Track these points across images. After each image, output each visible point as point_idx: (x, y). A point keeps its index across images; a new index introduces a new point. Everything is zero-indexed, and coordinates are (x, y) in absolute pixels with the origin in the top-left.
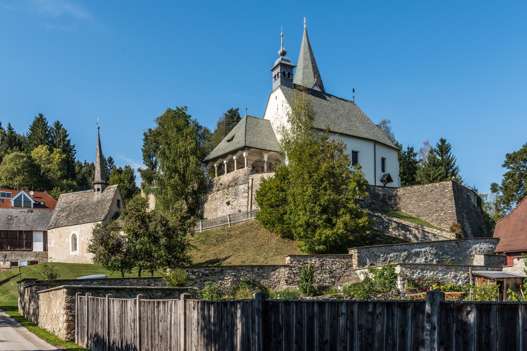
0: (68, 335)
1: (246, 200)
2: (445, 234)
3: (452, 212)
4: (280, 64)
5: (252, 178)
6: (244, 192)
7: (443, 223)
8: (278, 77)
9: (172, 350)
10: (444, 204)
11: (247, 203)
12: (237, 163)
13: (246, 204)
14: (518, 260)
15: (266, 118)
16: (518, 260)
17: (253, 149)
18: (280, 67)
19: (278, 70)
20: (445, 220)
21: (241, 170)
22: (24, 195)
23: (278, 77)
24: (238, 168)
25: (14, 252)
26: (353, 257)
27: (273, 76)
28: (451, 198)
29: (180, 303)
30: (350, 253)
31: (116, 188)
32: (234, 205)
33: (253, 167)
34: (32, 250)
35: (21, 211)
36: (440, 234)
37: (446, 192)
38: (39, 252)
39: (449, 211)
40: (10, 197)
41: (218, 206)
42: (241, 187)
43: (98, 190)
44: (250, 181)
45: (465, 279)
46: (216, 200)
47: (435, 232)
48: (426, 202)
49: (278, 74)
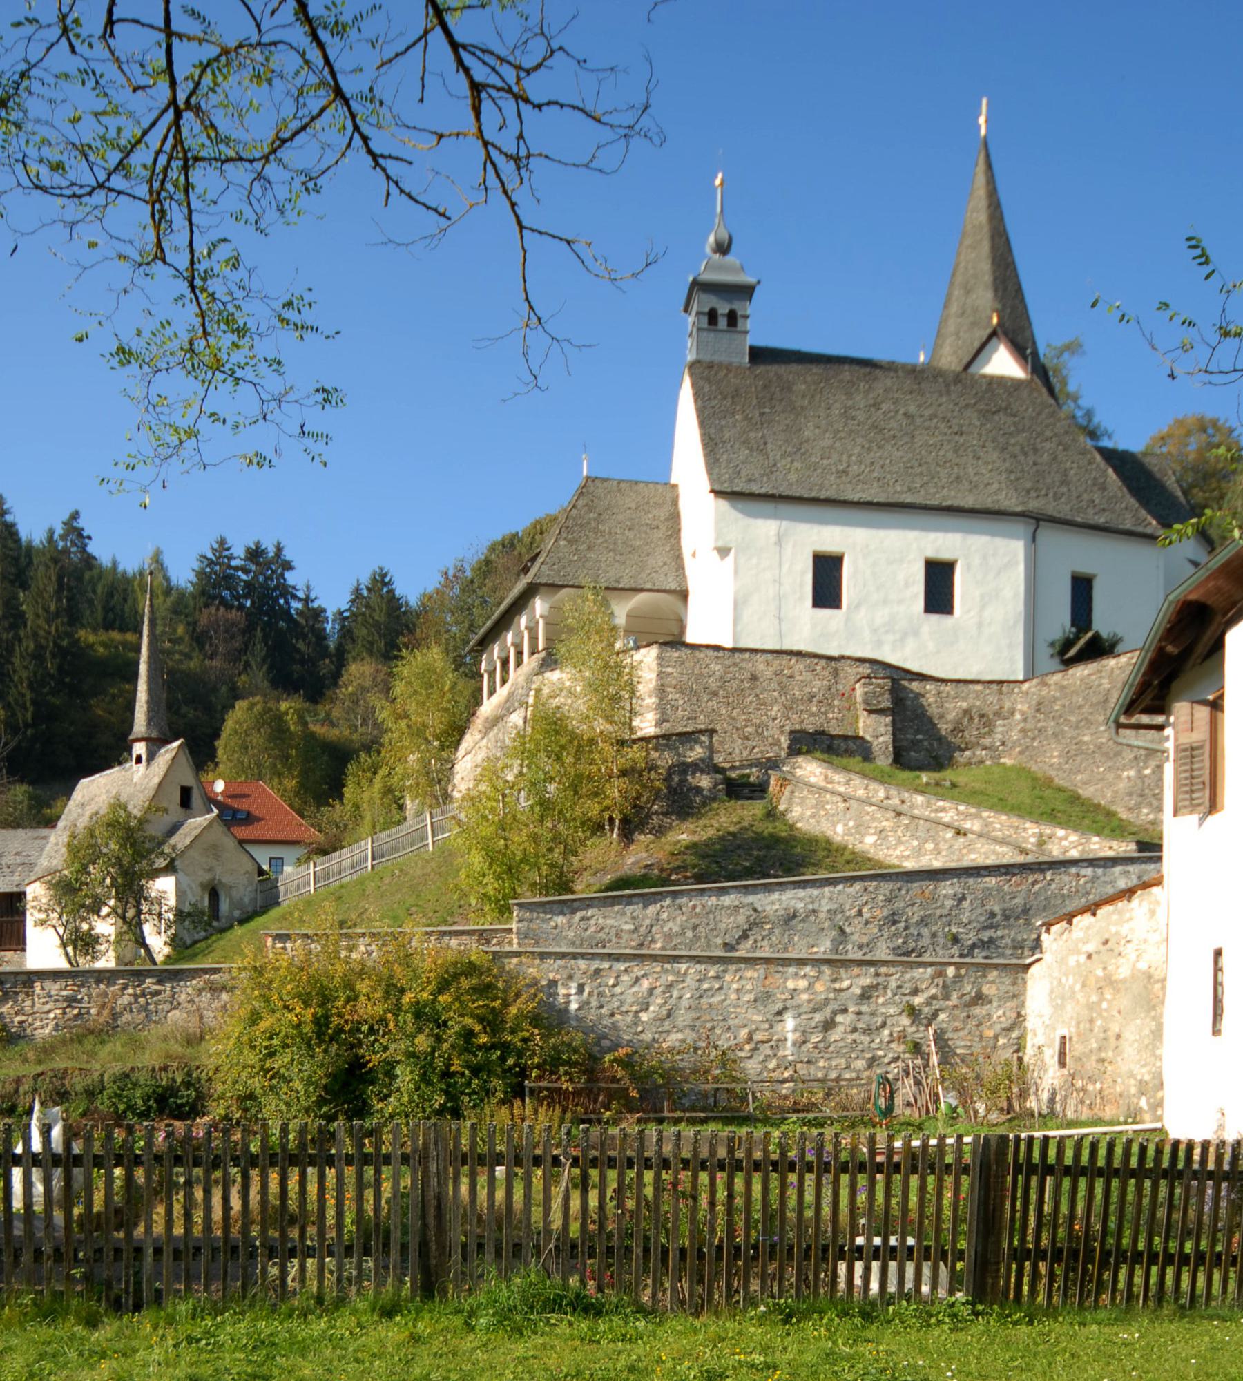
2: (1096, 846)
45: (815, 1010)
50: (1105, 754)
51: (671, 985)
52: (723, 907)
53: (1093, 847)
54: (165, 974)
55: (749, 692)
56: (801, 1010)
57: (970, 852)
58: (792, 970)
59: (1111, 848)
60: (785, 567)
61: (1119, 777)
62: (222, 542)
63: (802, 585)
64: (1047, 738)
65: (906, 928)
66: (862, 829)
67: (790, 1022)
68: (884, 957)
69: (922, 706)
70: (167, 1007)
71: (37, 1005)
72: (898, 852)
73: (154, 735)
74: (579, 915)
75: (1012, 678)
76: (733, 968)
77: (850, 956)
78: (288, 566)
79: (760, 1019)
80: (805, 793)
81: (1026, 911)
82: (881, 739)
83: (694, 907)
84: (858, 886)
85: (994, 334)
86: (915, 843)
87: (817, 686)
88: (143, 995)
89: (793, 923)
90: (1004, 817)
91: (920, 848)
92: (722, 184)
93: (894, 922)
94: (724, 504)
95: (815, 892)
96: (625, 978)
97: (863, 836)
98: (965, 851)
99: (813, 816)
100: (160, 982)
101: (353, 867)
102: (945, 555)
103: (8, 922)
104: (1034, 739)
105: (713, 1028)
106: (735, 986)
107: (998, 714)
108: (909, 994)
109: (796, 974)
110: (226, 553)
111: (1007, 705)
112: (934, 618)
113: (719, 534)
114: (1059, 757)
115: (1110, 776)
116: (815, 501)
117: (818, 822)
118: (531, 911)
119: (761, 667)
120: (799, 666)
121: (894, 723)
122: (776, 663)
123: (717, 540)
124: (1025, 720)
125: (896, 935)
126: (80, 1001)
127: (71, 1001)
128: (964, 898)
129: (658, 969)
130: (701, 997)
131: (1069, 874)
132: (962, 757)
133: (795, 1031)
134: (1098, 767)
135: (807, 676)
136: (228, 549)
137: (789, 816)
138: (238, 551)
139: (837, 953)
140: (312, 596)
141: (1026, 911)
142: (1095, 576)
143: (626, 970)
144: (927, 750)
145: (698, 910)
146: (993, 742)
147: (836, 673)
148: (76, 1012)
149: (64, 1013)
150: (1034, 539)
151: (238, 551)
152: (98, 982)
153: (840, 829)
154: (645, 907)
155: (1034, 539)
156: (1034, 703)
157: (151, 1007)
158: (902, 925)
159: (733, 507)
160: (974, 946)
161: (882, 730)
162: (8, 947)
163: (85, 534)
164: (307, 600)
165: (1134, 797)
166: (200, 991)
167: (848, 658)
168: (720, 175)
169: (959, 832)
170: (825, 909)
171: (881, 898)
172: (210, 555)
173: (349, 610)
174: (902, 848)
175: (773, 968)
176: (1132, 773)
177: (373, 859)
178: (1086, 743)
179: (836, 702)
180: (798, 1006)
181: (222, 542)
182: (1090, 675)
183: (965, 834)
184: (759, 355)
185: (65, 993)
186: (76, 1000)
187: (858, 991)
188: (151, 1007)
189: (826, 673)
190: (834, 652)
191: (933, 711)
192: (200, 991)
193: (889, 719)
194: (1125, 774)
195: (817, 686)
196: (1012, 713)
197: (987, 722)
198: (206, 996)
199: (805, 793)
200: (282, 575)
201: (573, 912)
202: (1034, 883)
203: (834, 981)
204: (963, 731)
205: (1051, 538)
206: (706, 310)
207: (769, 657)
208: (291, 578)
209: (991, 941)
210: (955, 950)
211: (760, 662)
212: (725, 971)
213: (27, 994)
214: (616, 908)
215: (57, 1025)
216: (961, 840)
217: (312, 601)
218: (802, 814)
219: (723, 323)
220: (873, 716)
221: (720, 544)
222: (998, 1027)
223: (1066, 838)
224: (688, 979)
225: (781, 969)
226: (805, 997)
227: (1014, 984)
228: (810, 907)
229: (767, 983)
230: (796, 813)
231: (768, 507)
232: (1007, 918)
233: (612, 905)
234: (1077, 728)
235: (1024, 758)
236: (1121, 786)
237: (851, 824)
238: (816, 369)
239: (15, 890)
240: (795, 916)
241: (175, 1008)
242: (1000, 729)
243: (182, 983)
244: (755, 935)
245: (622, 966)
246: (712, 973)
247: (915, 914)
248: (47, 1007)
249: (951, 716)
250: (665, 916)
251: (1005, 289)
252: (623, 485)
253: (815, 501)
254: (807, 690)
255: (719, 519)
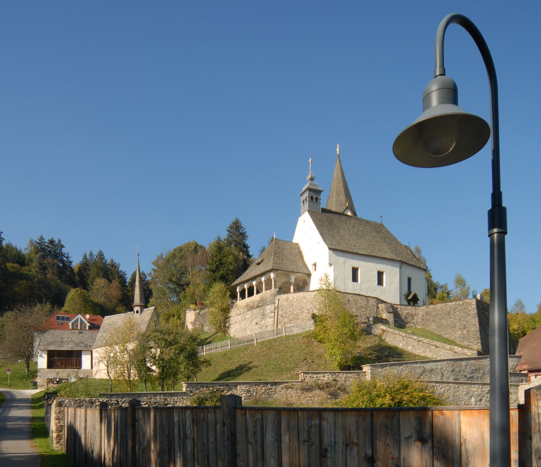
0: (57, 444)
1: (273, 319)
2: (466, 351)
3: (476, 330)
4: (309, 189)
5: (278, 298)
6: (271, 312)
7: (466, 340)
8: (306, 201)
9: (271, 462)
10: (467, 322)
11: (273, 322)
12: (265, 284)
13: (272, 323)
14: (536, 377)
15: (294, 241)
16: (536, 377)
17: (280, 271)
18: (308, 192)
19: (306, 195)
20: (468, 338)
21: (268, 291)
22: (80, 318)
23: (306, 201)
24: (266, 290)
25: (65, 370)
26: (366, 374)
27: (302, 200)
28: (475, 316)
29: (83, 410)
30: (364, 370)
31: (152, 311)
32: (261, 325)
33: (280, 289)
34: (81, 368)
35: (72, 332)
36: (462, 352)
37: (469, 310)
38: (87, 370)
39: (473, 329)
40: (69, 320)
41: (248, 326)
42: (268, 307)
43: (137, 312)
44: (277, 301)
45: (478, 396)
46: (246, 320)
47: (456, 349)
48: (449, 320)
49: (306, 199)
50: (451, 327)
51: (448, 390)
52: (417, 367)
53: (465, 352)
54: (273, 384)
55: (347, 304)
56: (476, 396)
57: (440, 352)
58: (473, 386)
59: (470, 352)
60: (346, 270)
61: (456, 333)
62: (42, 237)
64: (430, 322)
65: (456, 373)
66: (408, 345)
67: (473, 400)
68: (452, 381)
69: (397, 311)
70: (274, 393)
71: (238, 392)
72: (418, 351)
73: (143, 305)
74: (384, 368)
75: (397, 304)
76: (461, 385)
77: (444, 381)
78: (62, 246)
79: (467, 398)
80: (390, 334)
81: (479, 369)
82: (391, 320)
83: (411, 367)
84: (446, 362)
85: (347, 208)
86: (424, 349)
87: (364, 304)
88: (267, 389)
89: (432, 371)
90: (440, 343)
91: (425, 350)
92: (311, 161)
93: (454, 372)
94: (331, 252)
95: (437, 363)
96: (438, 388)
97: (408, 346)
98: (438, 352)
99: (392, 341)
100: (272, 386)
101: (222, 347)
102: (382, 270)
103: (67, 359)
104: (426, 322)
105: (457, 401)
106: (462, 390)
107: (415, 314)
109: (474, 387)
110: (43, 241)
111: (417, 312)
112: (380, 286)
113: (330, 260)
114: (436, 326)
115: (453, 333)
116: (353, 253)
117: (394, 342)
118: (374, 367)
119: (350, 298)
120: (359, 298)
121: (394, 315)
122: (354, 297)
123: (329, 262)
124: (423, 316)
125: (454, 375)
126: (251, 391)
127: (248, 391)
128: (467, 366)
129: (446, 385)
130: (455, 393)
131: (487, 360)
132: (408, 325)
133: (474, 401)
134: (449, 330)
135: (361, 301)
136: (44, 240)
137: (385, 340)
138: (47, 240)
139: (442, 380)
140: (69, 256)
141: (479, 369)
142: (408, 277)
143: (439, 386)
144: (399, 323)
145: (411, 368)
146: (414, 322)
147: (368, 301)
148: (250, 394)
149: (247, 395)
150: (401, 268)
151: (47, 240)
152: (255, 385)
153: (401, 344)
154: (400, 367)
155: (401, 268)
156: (425, 312)
157: (270, 393)
158: (455, 372)
159: (333, 253)
160: (469, 378)
161: (391, 317)
162: (67, 367)
164: (68, 258)
165: (461, 338)
166: (282, 388)
167: (371, 297)
168: (310, 159)
169: (437, 347)
170: (439, 368)
171: (451, 365)
172: (38, 241)
173: (82, 261)
174: (420, 350)
175: (470, 385)
176: (460, 332)
177: (230, 346)
178: (444, 324)
179: (368, 308)
180: (475, 395)
181: (42, 237)
182: (443, 306)
183: (438, 347)
184: (324, 211)
185: (247, 389)
186: (249, 391)
187: (487, 391)
188: (270, 393)
189: (365, 300)
190: (368, 295)
191: (400, 313)
192: (282, 388)
193: (393, 314)
194: (458, 332)
195: (364, 304)
196: (418, 314)
197: (413, 316)
198: (284, 390)
199: (390, 334)
200: (61, 250)
201: (383, 368)
202: (481, 362)
203: (482, 389)
204: (407, 318)
205: (404, 267)
206: (311, 196)
207: (352, 295)
208: (64, 250)
209: (473, 377)
210: (465, 379)
211: (350, 297)
212: (460, 386)
213: (235, 389)
214: (393, 367)
215: (245, 398)
216: (437, 349)
217: (69, 258)
218: (389, 340)
219: (314, 200)
220: (389, 313)
221: (330, 263)
222: (514, 400)
223: (457, 349)
224: (452, 388)
225: (471, 385)
226: (476, 393)
227: (516, 390)
228: (436, 367)
229: (468, 389)
230: (387, 340)
231: (341, 253)
232: (475, 371)
233: (392, 366)
234: (440, 319)
235: (423, 327)
236: (457, 335)
237: (404, 343)
239: (71, 349)
240: (433, 370)
241: (276, 393)
242: (416, 318)
243: (277, 386)
244: (424, 374)
245: (438, 385)
246: (457, 387)
247: (457, 370)
248: (242, 393)
249: (404, 314)
250: (404, 369)
251: (348, 196)
252: (285, 242)
253: (353, 253)
254: (361, 305)
255: (330, 256)
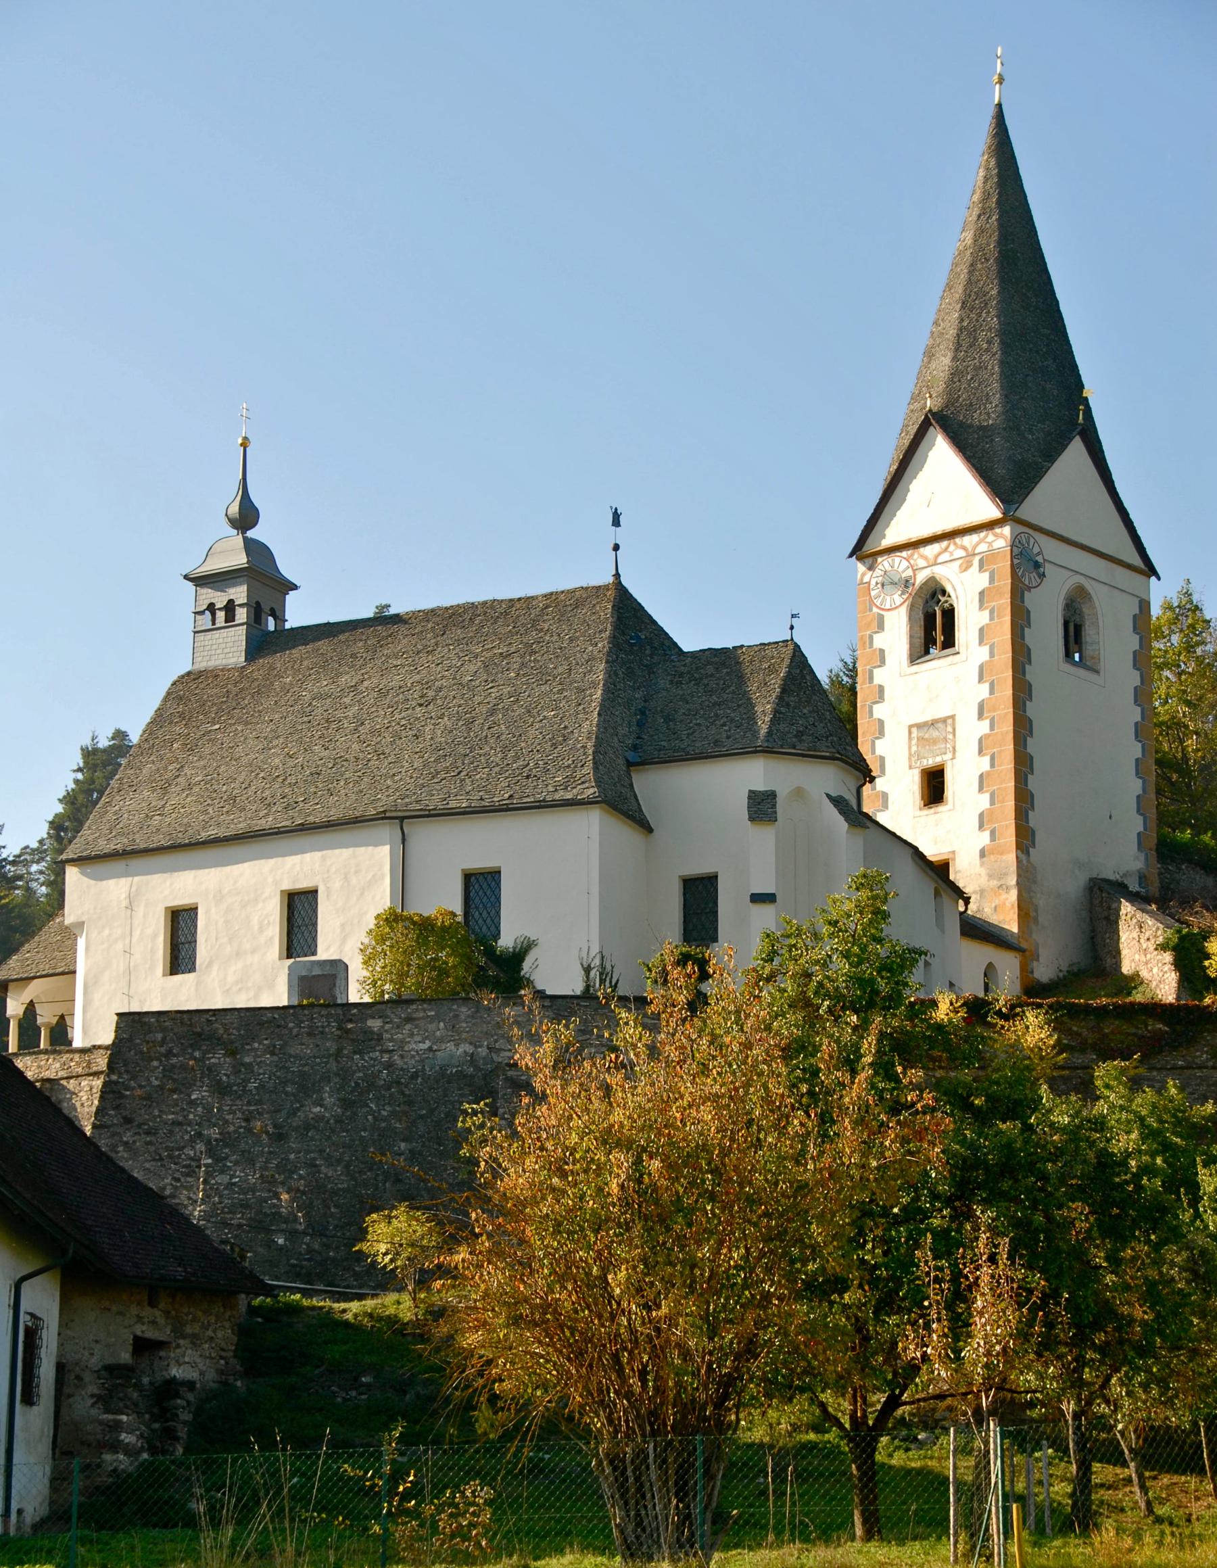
60: (137, 934)
63: (153, 951)
108: (439, 1248)
163: (35, 845)
231: (120, 865)
238: (323, 645)
